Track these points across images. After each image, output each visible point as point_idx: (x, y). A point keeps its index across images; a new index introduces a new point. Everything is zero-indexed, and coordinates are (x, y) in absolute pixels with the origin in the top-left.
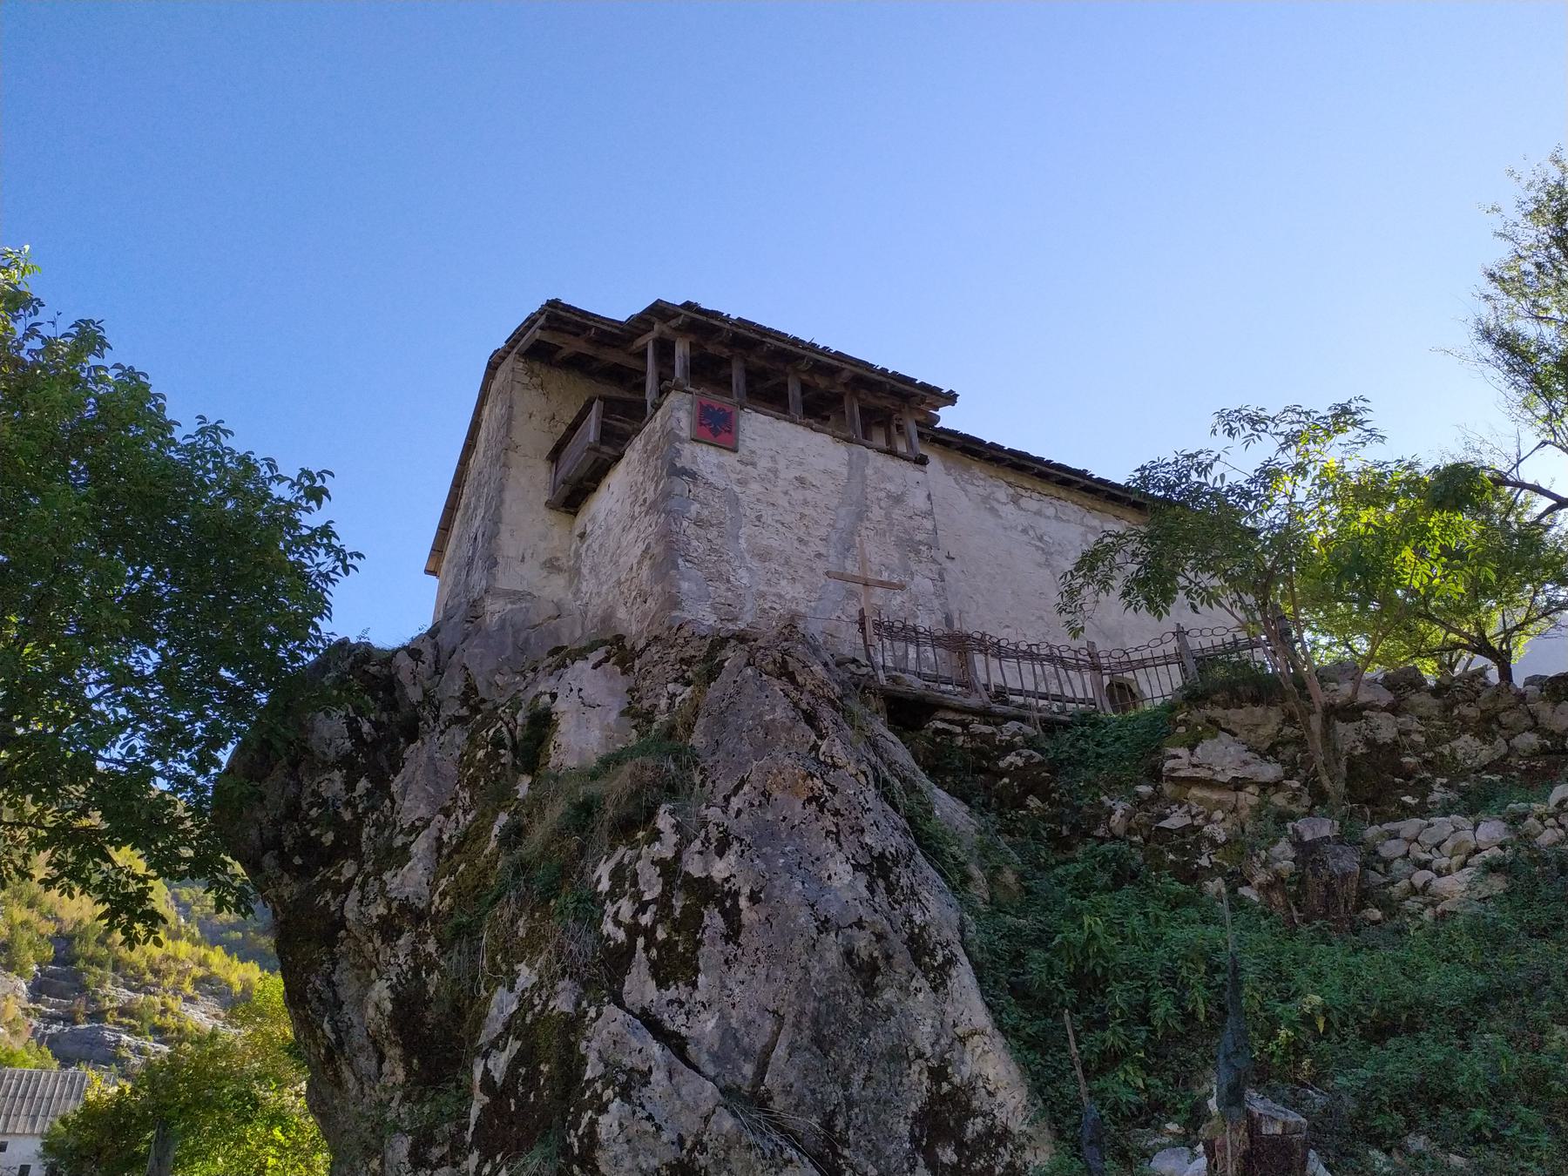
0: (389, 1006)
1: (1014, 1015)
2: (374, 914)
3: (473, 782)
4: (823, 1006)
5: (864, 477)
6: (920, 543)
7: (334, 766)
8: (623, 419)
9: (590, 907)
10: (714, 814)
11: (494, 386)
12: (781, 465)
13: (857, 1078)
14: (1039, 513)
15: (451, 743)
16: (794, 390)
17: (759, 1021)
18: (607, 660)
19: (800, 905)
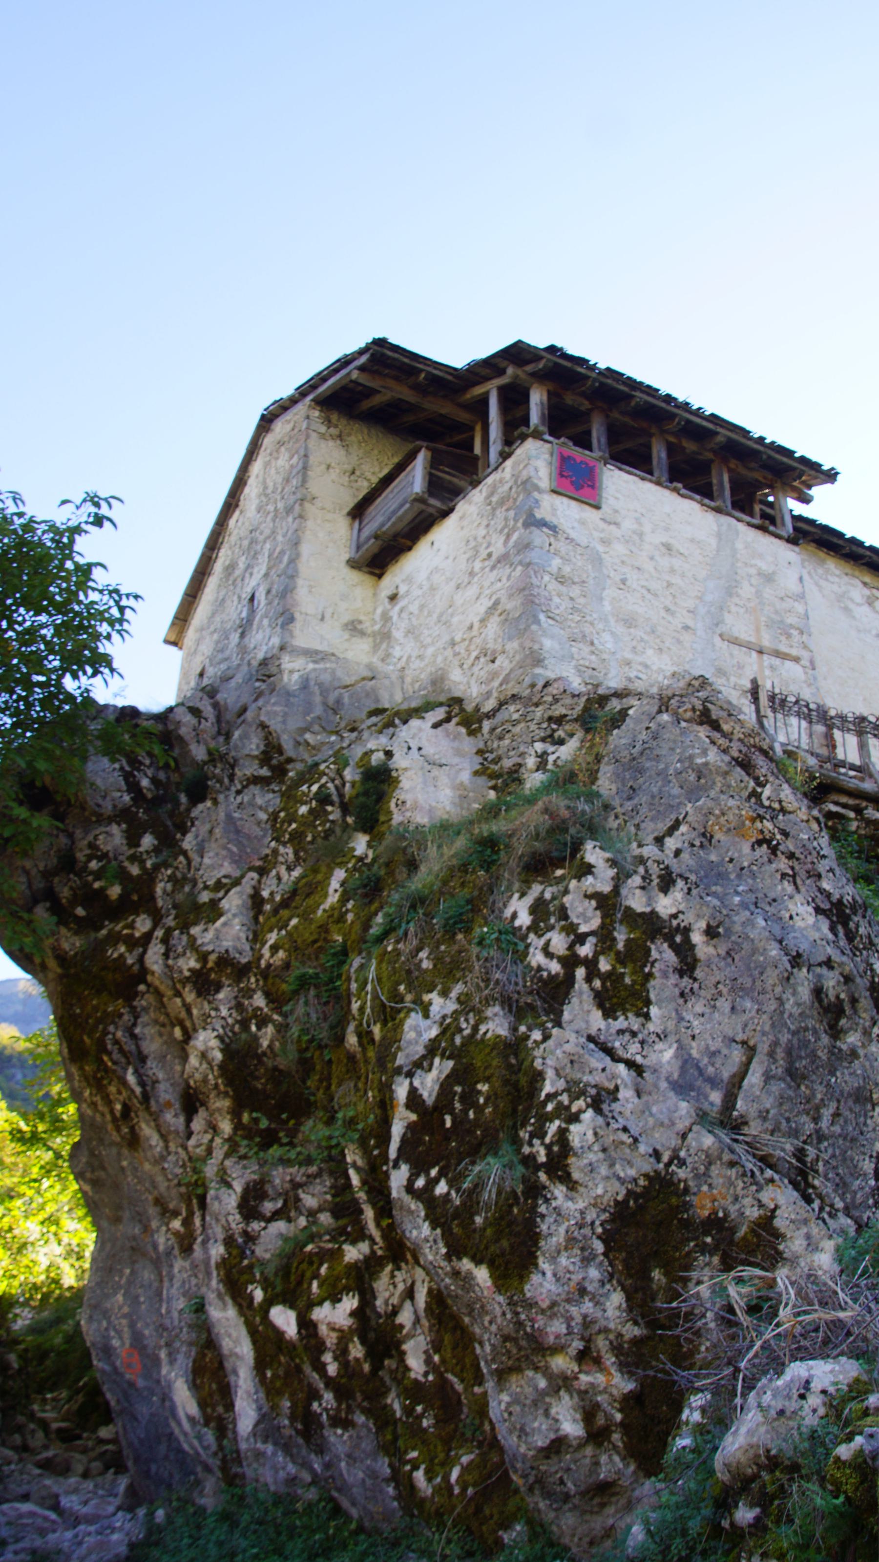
0: (218, 1056)
2: (185, 968)
3: (296, 838)
4: (795, 1041)
6: (791, 626)
7: (110, 820)
8: (457, 468)
9: (513, 942)
10: (649, 850)
11: (268, 440)
12: (647, 528)
13: (827, 1114)
15: (252, 803)
16: (659, 453)
17: (725, 1051)
18: (448, 720)
19: (768, 939)
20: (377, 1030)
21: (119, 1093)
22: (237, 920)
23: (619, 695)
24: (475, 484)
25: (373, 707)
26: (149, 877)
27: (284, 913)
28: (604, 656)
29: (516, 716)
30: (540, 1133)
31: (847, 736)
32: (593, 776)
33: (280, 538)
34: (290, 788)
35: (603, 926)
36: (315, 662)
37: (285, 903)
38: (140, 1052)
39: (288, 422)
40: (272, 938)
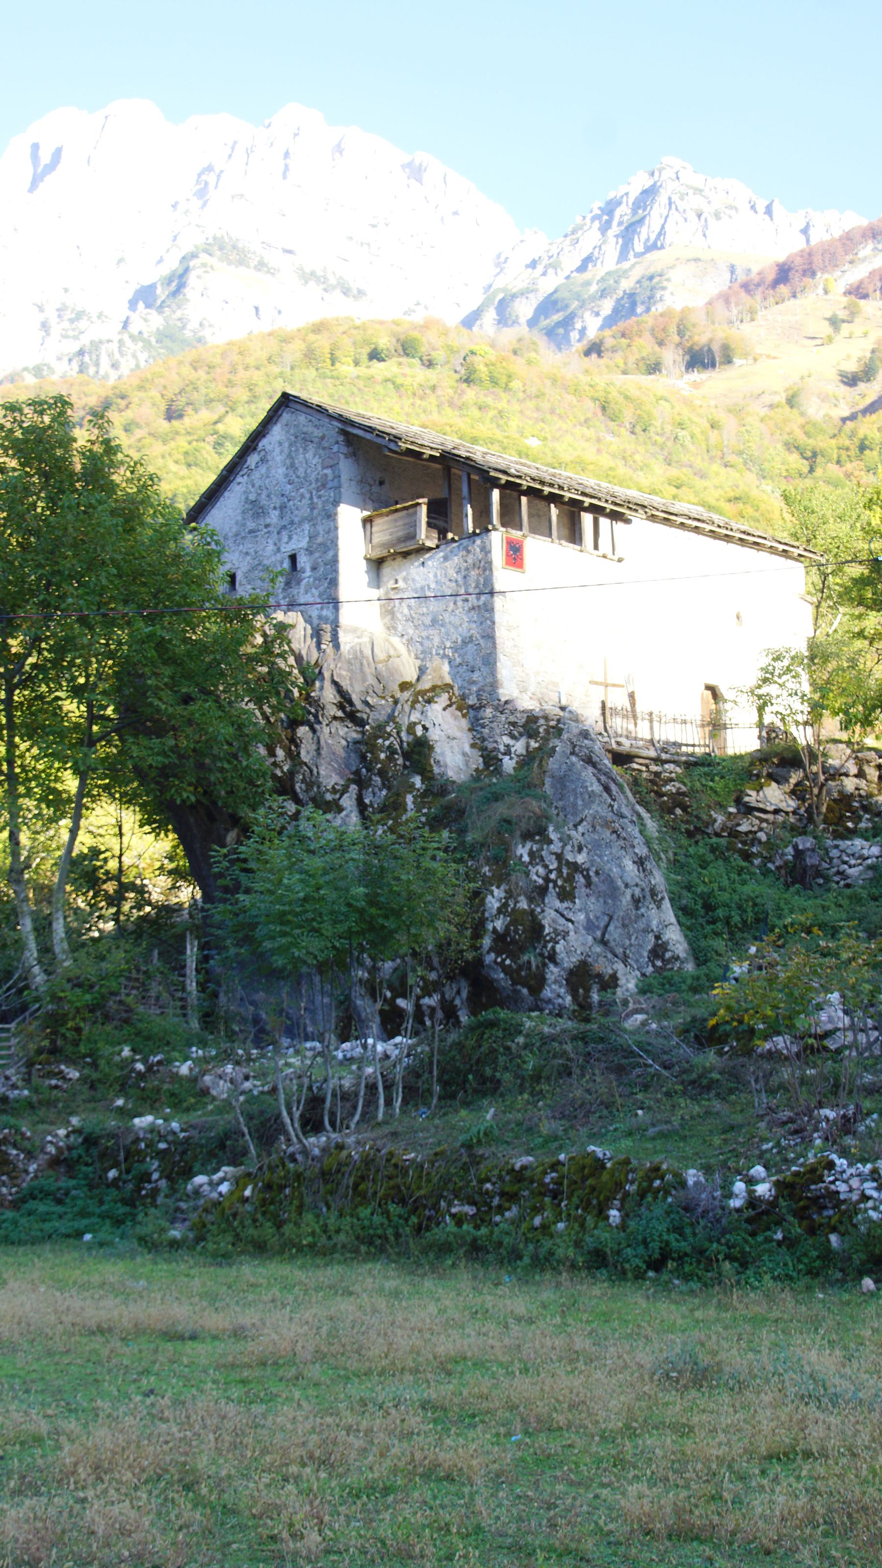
1: (683, 920)
30: (545, 947)
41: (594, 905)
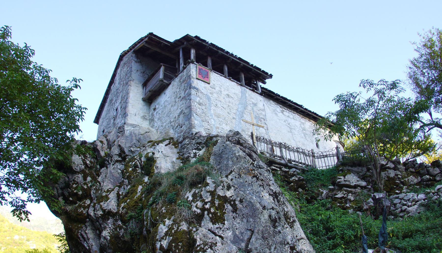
3: (129, 178)
4: (264, 229)
5: (246, 97)
7: (79, 173)
8: (173, 71)
11: (122, 63)
12: (222, 90)
13: (273, 248)
14: (288, 117)
16: (226, 68)
18: (169, 144)
20: (151, 230)
21: (83, 249)
22: (113, 201)
23: (217, 136)
24: (176, 76)
25: (149, 140)
26: (90, 189)
27: (126, 198)
28: (212, 126)
29: (188, 142)
31: (277, 148)
32: (209, 159)
33: (124, 92)
34: (127, 163)
35: (212, 200)
36: (133, 127)
37: (126, 196)
38: (88, 237)
39: (127, 57)
40: (123, 205)
41: (240, 225)
